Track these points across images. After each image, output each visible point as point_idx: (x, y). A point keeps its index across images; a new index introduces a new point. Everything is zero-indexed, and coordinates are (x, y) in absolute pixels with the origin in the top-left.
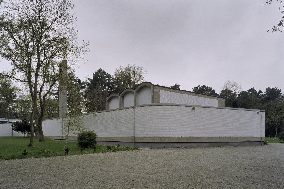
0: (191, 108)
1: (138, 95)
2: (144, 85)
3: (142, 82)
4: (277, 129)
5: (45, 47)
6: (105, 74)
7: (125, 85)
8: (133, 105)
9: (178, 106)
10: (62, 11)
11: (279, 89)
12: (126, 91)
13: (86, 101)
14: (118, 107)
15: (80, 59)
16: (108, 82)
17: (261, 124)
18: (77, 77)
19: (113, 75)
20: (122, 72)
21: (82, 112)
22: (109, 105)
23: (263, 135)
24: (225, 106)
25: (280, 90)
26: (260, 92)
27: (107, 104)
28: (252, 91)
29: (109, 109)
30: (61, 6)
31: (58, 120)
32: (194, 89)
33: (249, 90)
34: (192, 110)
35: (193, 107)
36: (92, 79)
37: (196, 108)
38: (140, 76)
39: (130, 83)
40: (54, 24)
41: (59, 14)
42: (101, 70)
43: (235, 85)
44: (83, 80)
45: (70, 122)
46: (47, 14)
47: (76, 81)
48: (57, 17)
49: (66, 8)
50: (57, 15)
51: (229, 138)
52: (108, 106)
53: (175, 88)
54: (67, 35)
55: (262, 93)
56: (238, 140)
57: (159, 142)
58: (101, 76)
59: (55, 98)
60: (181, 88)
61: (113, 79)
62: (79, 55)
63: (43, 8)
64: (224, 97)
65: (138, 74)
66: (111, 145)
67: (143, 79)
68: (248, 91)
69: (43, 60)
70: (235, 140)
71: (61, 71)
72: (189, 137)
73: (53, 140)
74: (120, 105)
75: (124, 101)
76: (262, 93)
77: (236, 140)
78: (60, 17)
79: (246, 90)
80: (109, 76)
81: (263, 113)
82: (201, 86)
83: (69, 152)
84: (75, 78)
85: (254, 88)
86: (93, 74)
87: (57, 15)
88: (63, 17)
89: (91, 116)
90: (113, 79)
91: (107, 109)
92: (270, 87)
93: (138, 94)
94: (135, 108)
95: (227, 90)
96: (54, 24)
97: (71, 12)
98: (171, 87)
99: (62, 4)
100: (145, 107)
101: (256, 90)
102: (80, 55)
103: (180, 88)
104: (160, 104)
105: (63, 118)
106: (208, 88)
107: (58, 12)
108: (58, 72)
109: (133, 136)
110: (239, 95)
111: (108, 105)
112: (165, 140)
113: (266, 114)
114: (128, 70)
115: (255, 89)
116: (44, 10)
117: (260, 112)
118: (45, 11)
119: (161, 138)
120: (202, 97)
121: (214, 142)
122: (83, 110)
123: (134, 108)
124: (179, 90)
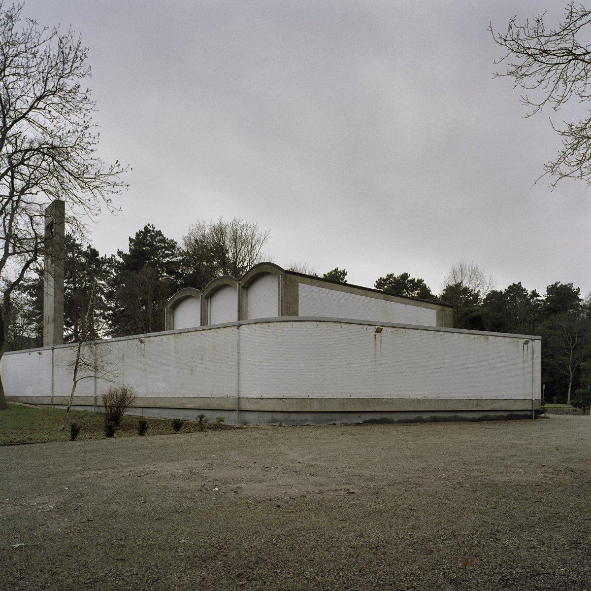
0: (373, 329)
1: (247, 295)
2: (262, 270)
3: (256, 262)
4: (570, 383)
5: (15, 167)
6: (163, 240)
7: (212, 270)
8: (233, 318)
9: (342, 324)
10: (59, 79)
11: (575, 287)
12: (216, 285)
13: (110, 309)
14: (197, 323)
15: (103, 204)
16: (169, 259)
17: (533, 369)
18: (89, 247)
19: (181, 245)
20: (203, 236)
21: (100, 335)
22: (174, 317)
23: (537, 395)
24: (452, 326)
25: (579, 290)
26: (535, 294)
27: (170, 317)
28: (516, 290)
29: (173, 329)
30: (57, 64)
31: (40, 354)
32: (381, 283)
33: (510, 287)
34: (376, 333)
35: (377, 327)
36: (128, 253)
37: (384, 329)
38: (250, 246)
39: (224, 262)
40: (36, 110)
41: (50, 85)
42: (152, 229)
43: (475, 274)
44: (105, 251)
45: (78, 360)
46: (18, 82)
47: (84, 254)
48: (45, 92)
49: (68, 71)
50: (45, 88)
51: (460, 401)
52: (172, 322)
53: (335, 279)
54: (71, 140)
55: (539, 298)
56: (480, 406)
57: (299, 410)
58: (151, 245)
59: (29, 297)
60: (349, 279)
61: (181, 254)
62: (101, 193)
63: (8, 66)
64: (449, 304)
65: (245, 242)
66: (180, 415)
67: (259, 255)
68: (506, 290)
69: (6, 200)
70: (473, 407)
71: (49, 227)
72: (369, 397)
73: (25, 407)
74: (201, 319)
75: (212, 305)
76: (539, 298)
77: (476, 407)
78: (53, 93)
79: (502, 287)
80: (172, 245)
81: (537, 345)
82: (397, 274)
83: (81, 435)
84: (84, 249)
85: (520, 283)
86: (131, 240)
87: (45, 88)
88: (61, 93)
89: (128, 345)
90: (181, 254)
91: (170, 329)
92: (556, 284)
93: (247, 292)
94: (241, 327)
95: (458, 285)
96: (35, 108)
97: (84, 83)
98: (324, 275)
99: (58, 61)
100: (264, 324)
101: (525, 289)
102: (104, 193)
103: (346, 281)
104: (300, 317)
105: (54, 349)
106: (412, 281)
107: (47, 79)
108: (42, 231)
109: (235, 395)
110: (485, 300)
111: (172, 318)
112: (311, 406)
113: (544, 346)
114: (220, 231)
115: (523, 286)
116: (13, 71)
117: (531, 341)
118: (14, 75)
119: (303, 400)
120: (399, 302)
121: (425, 410)
122: (103, 328)
123: (239, 327)
124: (345, 284)
